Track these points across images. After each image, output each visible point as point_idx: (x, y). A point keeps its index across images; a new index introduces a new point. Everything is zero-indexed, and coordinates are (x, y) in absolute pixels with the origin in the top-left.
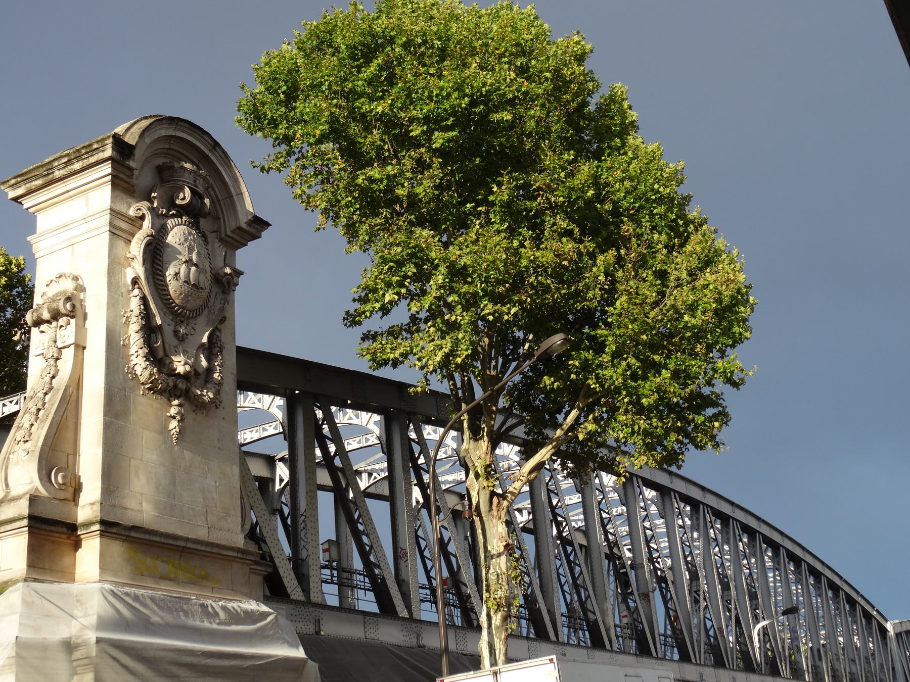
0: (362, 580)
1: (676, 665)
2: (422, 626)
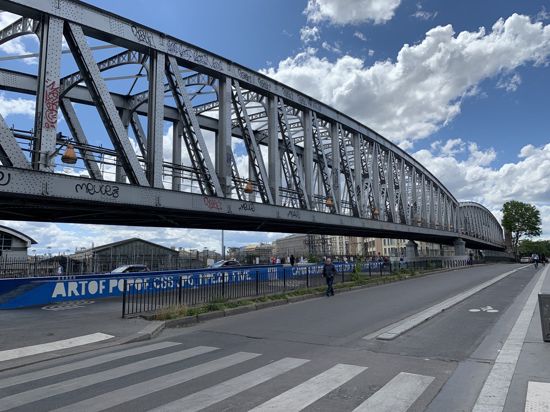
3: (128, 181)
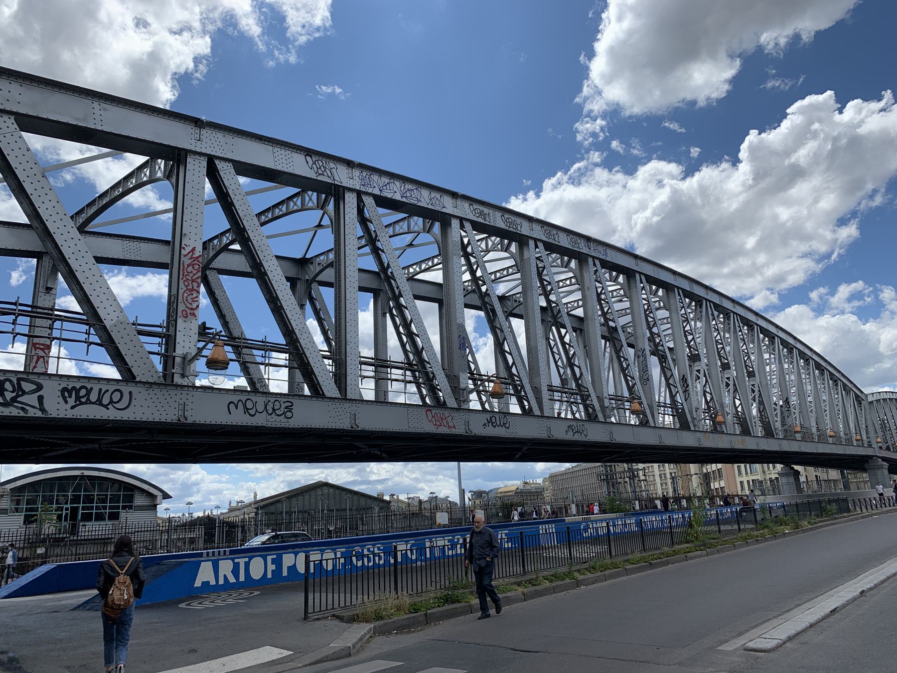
1: (740, 438)
3: (307, 391)
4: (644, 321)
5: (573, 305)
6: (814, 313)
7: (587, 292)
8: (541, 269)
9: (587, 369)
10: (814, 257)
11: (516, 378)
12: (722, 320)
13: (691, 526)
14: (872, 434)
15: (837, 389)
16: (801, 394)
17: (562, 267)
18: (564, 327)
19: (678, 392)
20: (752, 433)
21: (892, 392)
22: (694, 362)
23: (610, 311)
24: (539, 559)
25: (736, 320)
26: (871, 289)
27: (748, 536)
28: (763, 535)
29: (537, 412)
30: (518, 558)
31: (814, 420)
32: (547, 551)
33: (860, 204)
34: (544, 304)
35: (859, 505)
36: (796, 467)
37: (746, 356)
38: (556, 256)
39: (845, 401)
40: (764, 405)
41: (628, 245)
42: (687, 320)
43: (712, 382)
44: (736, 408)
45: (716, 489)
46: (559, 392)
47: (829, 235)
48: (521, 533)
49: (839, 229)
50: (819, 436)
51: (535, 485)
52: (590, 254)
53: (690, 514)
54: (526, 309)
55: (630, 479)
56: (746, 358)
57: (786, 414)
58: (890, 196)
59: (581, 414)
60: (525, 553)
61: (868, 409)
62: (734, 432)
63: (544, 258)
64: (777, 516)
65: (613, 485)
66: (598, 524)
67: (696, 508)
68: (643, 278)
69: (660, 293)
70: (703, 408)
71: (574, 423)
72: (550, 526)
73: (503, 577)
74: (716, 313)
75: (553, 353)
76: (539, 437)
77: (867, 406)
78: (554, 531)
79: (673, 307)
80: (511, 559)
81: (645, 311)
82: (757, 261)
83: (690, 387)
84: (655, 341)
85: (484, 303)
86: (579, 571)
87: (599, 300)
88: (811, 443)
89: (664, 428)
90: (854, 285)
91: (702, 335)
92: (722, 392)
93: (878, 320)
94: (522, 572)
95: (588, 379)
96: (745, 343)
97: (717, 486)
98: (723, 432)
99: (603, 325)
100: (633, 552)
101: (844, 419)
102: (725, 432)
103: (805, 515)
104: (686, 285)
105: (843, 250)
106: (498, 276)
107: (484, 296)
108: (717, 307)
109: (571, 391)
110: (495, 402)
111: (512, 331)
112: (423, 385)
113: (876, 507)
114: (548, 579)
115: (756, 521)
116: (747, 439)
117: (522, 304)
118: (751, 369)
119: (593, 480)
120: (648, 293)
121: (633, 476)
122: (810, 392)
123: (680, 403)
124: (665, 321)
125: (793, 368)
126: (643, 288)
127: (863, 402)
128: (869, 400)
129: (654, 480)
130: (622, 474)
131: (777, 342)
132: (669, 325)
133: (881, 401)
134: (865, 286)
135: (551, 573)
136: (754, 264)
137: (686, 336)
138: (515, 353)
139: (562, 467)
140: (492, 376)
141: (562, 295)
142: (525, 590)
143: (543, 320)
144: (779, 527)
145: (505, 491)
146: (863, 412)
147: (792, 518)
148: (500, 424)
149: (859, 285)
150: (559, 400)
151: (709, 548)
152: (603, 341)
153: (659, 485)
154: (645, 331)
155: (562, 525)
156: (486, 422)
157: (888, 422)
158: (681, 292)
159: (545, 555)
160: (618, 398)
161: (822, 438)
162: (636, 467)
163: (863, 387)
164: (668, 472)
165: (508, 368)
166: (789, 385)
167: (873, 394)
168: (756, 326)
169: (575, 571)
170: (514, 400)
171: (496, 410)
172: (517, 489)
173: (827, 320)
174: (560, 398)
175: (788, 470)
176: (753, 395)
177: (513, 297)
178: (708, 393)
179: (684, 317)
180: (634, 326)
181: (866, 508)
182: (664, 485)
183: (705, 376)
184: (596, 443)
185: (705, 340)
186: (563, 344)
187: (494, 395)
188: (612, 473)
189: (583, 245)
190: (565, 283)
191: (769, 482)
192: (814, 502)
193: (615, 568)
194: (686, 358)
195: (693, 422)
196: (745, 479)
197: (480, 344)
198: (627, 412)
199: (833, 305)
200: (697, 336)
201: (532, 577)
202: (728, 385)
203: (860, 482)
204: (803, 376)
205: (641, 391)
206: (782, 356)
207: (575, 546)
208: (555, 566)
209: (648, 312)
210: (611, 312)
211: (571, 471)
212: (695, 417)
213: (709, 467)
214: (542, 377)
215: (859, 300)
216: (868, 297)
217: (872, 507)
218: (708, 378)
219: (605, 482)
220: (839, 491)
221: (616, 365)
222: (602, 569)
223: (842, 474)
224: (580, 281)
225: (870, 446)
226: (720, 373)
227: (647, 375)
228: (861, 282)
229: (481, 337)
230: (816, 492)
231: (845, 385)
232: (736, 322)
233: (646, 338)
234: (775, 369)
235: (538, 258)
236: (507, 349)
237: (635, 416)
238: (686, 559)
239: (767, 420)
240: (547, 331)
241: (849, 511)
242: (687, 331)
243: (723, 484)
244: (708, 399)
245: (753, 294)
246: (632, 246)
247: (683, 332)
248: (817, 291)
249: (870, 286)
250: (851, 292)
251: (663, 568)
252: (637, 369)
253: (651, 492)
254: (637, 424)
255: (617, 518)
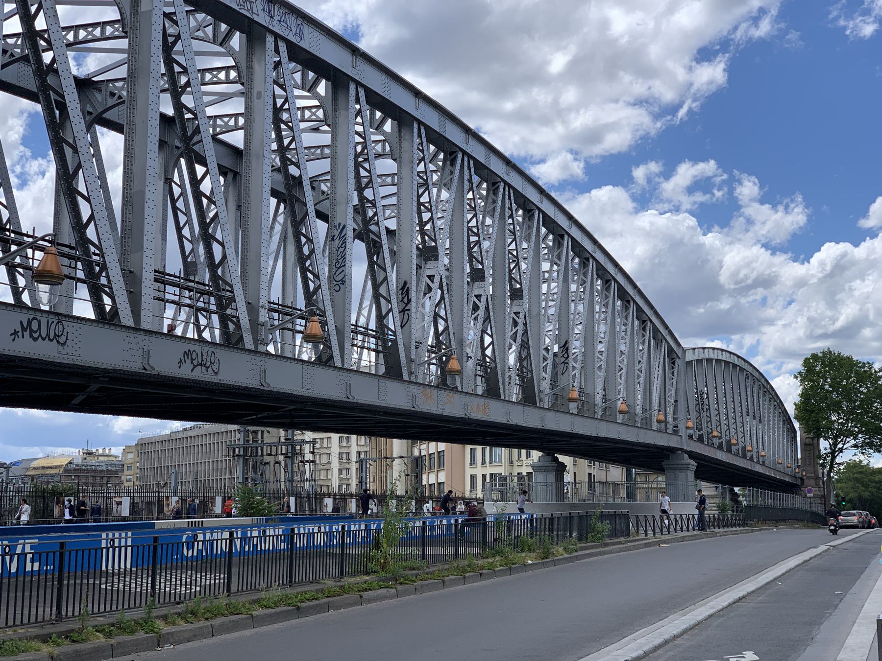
0: (177, 293)
1: (482, 401)
2: (267, 360)
4: (352, 175)
5: (226, 123)
6: (634, 205)
7: (256, 103)
8: (171, 40)
9: (237, 252)
10: (651, 108)
11: (92, 249)
12: (484, 193)
13: (377, 545)
14: (682, 414)
15: (644, 336)
16: (589, 337)
17: (214, 42)
18: (204, 163)
19: (391, 310)
20: (502, 394)
21: (722, 350)
22: (427, 260)
23: (293, 146)
24: (90, 593)
25: (507, 197)
26: (725, 176)
27: (469, 566)
28: (491, 567)
29: (127, 318)
30: (49, 591)
31: (602, 383)
32: (110, 580)
33: (736, 28)
34: (170, 111)
35: (644, 525)
36: (562, 458)
37: (514, 261)
38: (204, 20)
39: (652, 356)
40: (528, 349)
41: (349, 26)
42: (426, 185)
43: (451, 301)
44: (483, 349)
45: (430, 485)
46: (178, 286)
47: (681, 74)
48: (62, 545)
49: (698, 66)
50: (604, 410)
51: (106, 459)
52: (271, 27)
53: (379, 525)
54: (131, 115)
55: (286, 457)
56: (512, 266)
57: (560, 368)
58: (782, 25)
59: (213, 333)
60: (66, 582)
61: (682, 374)
62: (475, 389)
63: (180, 17)
64: (518, 536)
65: (254, 467)
66: (215, 535)
67: (393, 515)
68: (362, 93)
69: (388, 126)
70: (430, 343)
71: (197, 348)
72: (123, 535)
73: (14, 625)
74: (476, 179)
75: (175, 210)
76: (125, 368)
77: (682, 369)
78: (129, 543)
79: (406, 157)
80: (20, 594)
81: (357, 156)
82: (561, 100)
83: (413, 304)
84: (365, 214)
85: (45, 88)
86: (165, 618)
87: (277, 121)
88: (590, 420)
89: (357, 372)
90: (701, 166)
91: (448, 215)
92: (465, 320)
93: (726, 230)
94: (54, 617)
95: (234, 271)
96: (515, 240)
97: (432, 481)
98: (455, 389)
99: (278, 170)
100: (269, 587)
101: (645, 386)
102: (459, 389)
103: (561, 538)
104: (432, 120)
105: (698, 103)
106: (81, 37)
107: (44, 72)
108: (480, 168)
109: (201, 287)
110: (43, 289)
111: (98, 155)
112: (21, 270)
113: (668, 530)
114: (104, 630)
115: (485, 542)
116: (493, 404)
117: (124, 102)
118: (518, 286)
119: (220, 455)
120: (367, 123)
121: (293, 452)
122: (602, 335)
123: (392, 331)
124: (389, 180)
125: (584, 292)
126: (359, 113)
127: (678, 362)
128: (687, 360)
129: (329, 463)
130: (274, 448)
131: (565, 244)
132: (394, 189)
133: (705, 361)
134: (717, 170)
135: (112, 620)
136: (556, 102)
137: (420, 213)
138: (98, 196)
139: (164, 428)
140: (43, 239)
141: (206, 99)
142: (56, 651)
143: (162, 144)
144: (519, 555)
145: (45, 465)
146: (675, 377)
147: (541, 541)
148: (48, 335)
149: (709, 167)
150: (173, 302)
151: (401, 584)
152: (273, 201)
153: (335, 472)
154: (350, 193)
155: (149, 533)
156: (19, 329)
157: (708, 397)
158: (423, 131)
159: (103, 586)
160: (285, 310)
161: (609, 414)
162: (301, 437)
163: (681, 338)
164: (354, 450)
165: (79, 227)
166: (573, 320)
167: (694, 349)
168: (537, 213)
169: (157, 617)
170: (83, 291)
171: (43, 307)
172: (70, 463)
173: (652, 219)
174: (176, 298)
175: (548, 463)
176: (514, 330)
177: (107, 86)
178: (488, 334)
179: (421, 178)
180: (333, 181)
181: (654, 531)
182: (344, 472)
183: (441, 288)
184: (234, 387)
185: (451, 225)
186: (198, 195)
187: (40, 276)
188: (255, 444)
189: (260, 7)
190: (216, 76)
191: (516, 479)
192: (579, 516)
193: (232, 614)
194: (415, 251)
195: (409, 367)
196: (479, 471)
197: (32, 172)
198: (299, 338)
199: (665, 195)
200: (439, 215)
201: (71, 626)
202: (476, 308)
203: (652, 488)
204: (597, 308)
205: (328, 303)
206: (570, 269)
207: (163, 572)
208: (120, 607)
209: (361, 159)
210: (295, 149)
211: (181, 435)
212: (413, 357)
213: (424, 446)
214: (147, 253)
215: (705, 192)
216: (719, 190)
217: (661, 530)
218: (446, 292)
219: (241, 460)
220: (620, 501)
221: (291, 248)
222: (208, 615)
223: (629, 474)
224: (245, 78)
225: (676, 432)
226: (466, 286)
227: (343, 273)
228: (712, 163)
229: (35, 157)
230: (584, 500)
231: (656, 330)
232: (507, 201)
233: (351, 205)
234: (555, 291)
235: (166, 15)
236: (82, 188)
237: (310, 346)
238: (361, 601)
239: (530, 375)
240: (169, 166)
241: (627, 534)
242: (423, 204)
243: (442, 477)
244: (441, 328)
245: (547, 155)
246: (356, 32)
247: (415, 204)
248: (645, 166)
249: (724, 172)
250: (695, 177)
251: (318, 615)
252: (327, 260)
253: (319, 483)
254: (313, 359)
255: (252, 526)
